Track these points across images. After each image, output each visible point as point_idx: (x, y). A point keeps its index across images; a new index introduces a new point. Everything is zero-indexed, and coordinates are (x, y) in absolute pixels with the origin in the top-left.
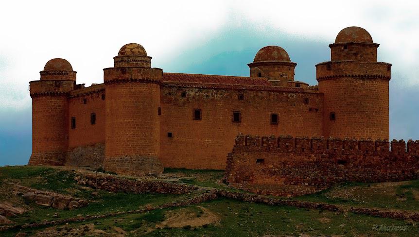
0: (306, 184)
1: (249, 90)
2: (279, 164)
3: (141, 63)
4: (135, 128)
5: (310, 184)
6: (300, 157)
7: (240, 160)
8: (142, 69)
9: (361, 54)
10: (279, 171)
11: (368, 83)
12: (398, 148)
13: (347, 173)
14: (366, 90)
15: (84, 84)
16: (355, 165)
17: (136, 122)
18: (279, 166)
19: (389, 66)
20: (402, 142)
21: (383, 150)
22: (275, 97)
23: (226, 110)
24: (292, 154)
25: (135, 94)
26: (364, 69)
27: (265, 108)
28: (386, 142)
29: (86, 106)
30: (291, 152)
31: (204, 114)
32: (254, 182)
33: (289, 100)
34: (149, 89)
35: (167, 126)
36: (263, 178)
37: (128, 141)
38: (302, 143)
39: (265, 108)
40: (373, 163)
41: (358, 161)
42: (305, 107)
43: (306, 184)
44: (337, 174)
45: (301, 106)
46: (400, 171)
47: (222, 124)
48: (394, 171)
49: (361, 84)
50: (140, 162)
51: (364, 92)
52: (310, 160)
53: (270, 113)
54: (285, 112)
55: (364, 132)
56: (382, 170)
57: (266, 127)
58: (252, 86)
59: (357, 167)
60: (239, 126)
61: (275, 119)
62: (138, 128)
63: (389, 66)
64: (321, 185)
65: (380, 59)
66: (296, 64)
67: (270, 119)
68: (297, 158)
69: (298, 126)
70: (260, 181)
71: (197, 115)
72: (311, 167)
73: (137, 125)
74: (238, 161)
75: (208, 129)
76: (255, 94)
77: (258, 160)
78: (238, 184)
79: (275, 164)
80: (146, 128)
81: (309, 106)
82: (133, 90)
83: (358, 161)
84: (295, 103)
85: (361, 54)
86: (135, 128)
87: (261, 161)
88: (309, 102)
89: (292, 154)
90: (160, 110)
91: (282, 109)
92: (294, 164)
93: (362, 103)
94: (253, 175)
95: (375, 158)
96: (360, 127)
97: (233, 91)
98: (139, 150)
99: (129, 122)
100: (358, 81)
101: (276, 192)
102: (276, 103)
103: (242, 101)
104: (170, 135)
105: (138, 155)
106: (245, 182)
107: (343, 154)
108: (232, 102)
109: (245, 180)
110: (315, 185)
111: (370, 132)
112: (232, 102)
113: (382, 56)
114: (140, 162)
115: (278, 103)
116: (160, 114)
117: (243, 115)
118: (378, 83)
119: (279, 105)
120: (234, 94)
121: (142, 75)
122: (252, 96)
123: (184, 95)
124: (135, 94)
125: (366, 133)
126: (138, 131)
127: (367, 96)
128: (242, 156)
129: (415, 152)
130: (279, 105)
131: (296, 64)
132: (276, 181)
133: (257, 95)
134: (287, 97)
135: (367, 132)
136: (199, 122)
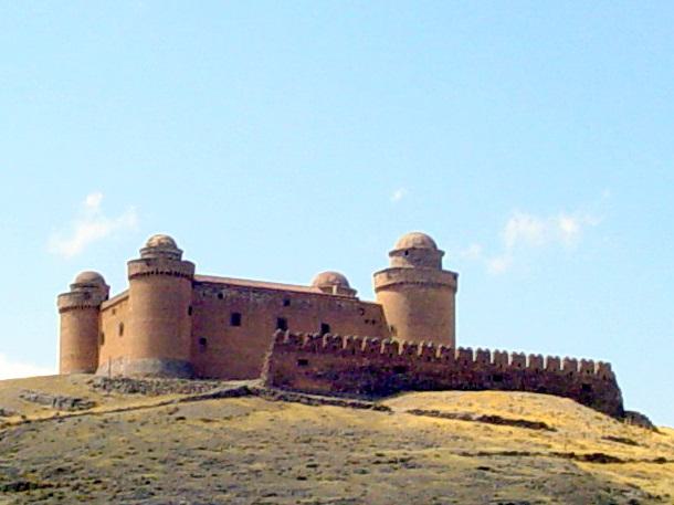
5: (361, 392)
11: (432, 292)
19: (455, 276)
20: (469, 351)
28: (451, 350)
29: (114, 317)
31: (243, 319)
58: (396, 452)
63: (455, 276)
65: (445, 267)
71: (236, 320)
81: (365, 317)
87: (303, 363)
90: (190, 309)
94: (294, 379)
104: (203, 341)
113: (447, 264)
116: (190, 313)
118: (444, 293)
123: (220, 296)
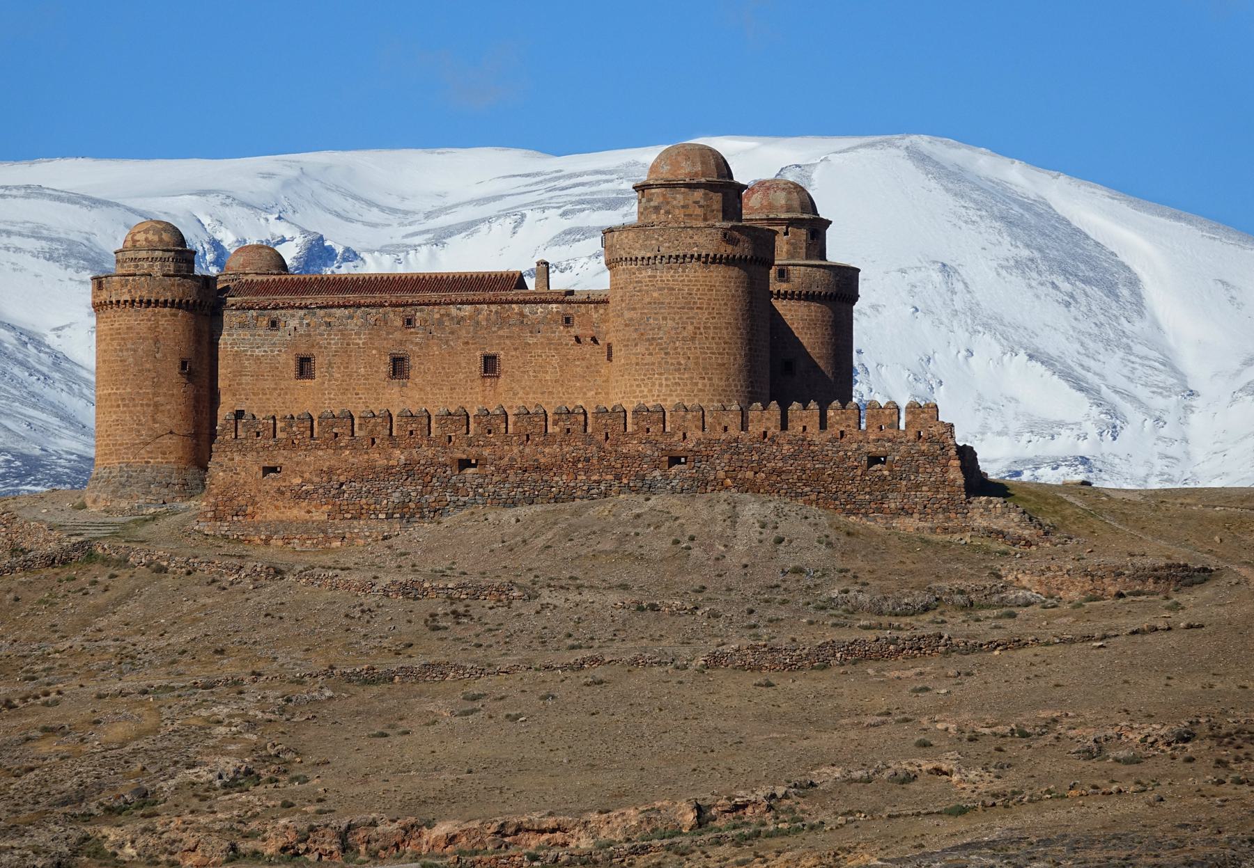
0: (380, 516)
1: (427, 305)
2: (317, 476)
3: (146, 265)
4: (118, 406)
5: (389, 516)
6: (366, 457)
7: (224, 471)
8: (131, 278)
9: (668, 207)
10: (315, 491)
12: (606, 425)
13: (480, 486)
14: (660, 289)
15: (1020, 266)
16: (498, 470)
17: (120, 394)
18: (316, 480)
21: (568, 430)
22: (493, 317)
23: (374, 352)
24: (348, 452)
25: (120, 334)
26: (654, 242)
27: (467, 343)
30: (346, 447)
31: (319, 362)
32: (258, 518)
33: (525, 320)
34: (150, 320)
35: (234, 395)
36: (277, 508)
37: (109, 435)
38: (370, 426)
39: (467, 343)
40: (542, 460)
41: (507, 459)
42: (564, 334)
43: (382, 516)
44: (456, 491)
45: (555, 332)
46: (610, 477)
47: (365, 384)
48: (595, 478)
49: (649, 277)
50: (123, 479)
51: (655, 294)
52: (391, 463)
53: (478, 353)
54: (516, 349)
55: (653, 384)
56: (564, 477)
57: (469, 383)
59: (505, 471)
60: (405, 385)
61: (490, 365)
62: (124, 405)
64: (418, 516)
66: (831, 222)
67: (479, 365)
68: (359, 460)
69: (548, 378)
70: (272, 515)
72: (391, 478)
73: (123, 399)
74: (221, 474)
75: (332, 396)
76: (442, 311)
77: (264, 468)
78: (219, 523)
79: (307, 475)
80: (142, 405)
82: (116, 325)
83: (507, 459)
84: (541, 327)
85: (668, 207)
86: (118, 406)
88: (576, 322)
89: (348, 452)
91: (508, 342)
92: (352, 473)
93: (651, 321)
94: (254, 503)
95: (547, 450)
96: (645, 375)
97: (389, 309)
98: (127, 454)
99: (110, 394)
100: (643, 272)
101: (305, 536)
102: (494, 329)
103: (412, 330)
105: (123, 465)
106: (235, 518)
107: (469, 446)
108: (388, 334)
109: (237, 515)
110: (402, 517)
111: (667, 385)
112: (388, 334)
114: (123, 479)
115: (499, 329)
117: (413, 361)
119: (501, 333)
120: (391, 315)
121: (130, 291)
122: (437, 316)
124: (120, 334)
125: (657, 387)
126: (125, 412)
127: (663, 303)
128: (230, 464)
129: (648, 430)
130: (501, 333)
131: (831, 222)
132: (309, 512)
133: (448, 315)
134: (522, 314)
135: (661, 385)
136: (308, 382)
